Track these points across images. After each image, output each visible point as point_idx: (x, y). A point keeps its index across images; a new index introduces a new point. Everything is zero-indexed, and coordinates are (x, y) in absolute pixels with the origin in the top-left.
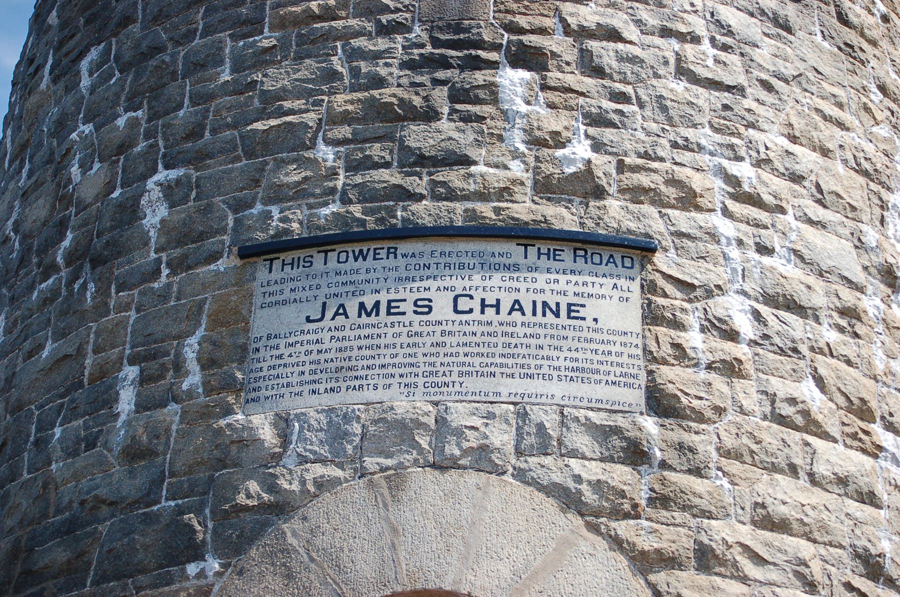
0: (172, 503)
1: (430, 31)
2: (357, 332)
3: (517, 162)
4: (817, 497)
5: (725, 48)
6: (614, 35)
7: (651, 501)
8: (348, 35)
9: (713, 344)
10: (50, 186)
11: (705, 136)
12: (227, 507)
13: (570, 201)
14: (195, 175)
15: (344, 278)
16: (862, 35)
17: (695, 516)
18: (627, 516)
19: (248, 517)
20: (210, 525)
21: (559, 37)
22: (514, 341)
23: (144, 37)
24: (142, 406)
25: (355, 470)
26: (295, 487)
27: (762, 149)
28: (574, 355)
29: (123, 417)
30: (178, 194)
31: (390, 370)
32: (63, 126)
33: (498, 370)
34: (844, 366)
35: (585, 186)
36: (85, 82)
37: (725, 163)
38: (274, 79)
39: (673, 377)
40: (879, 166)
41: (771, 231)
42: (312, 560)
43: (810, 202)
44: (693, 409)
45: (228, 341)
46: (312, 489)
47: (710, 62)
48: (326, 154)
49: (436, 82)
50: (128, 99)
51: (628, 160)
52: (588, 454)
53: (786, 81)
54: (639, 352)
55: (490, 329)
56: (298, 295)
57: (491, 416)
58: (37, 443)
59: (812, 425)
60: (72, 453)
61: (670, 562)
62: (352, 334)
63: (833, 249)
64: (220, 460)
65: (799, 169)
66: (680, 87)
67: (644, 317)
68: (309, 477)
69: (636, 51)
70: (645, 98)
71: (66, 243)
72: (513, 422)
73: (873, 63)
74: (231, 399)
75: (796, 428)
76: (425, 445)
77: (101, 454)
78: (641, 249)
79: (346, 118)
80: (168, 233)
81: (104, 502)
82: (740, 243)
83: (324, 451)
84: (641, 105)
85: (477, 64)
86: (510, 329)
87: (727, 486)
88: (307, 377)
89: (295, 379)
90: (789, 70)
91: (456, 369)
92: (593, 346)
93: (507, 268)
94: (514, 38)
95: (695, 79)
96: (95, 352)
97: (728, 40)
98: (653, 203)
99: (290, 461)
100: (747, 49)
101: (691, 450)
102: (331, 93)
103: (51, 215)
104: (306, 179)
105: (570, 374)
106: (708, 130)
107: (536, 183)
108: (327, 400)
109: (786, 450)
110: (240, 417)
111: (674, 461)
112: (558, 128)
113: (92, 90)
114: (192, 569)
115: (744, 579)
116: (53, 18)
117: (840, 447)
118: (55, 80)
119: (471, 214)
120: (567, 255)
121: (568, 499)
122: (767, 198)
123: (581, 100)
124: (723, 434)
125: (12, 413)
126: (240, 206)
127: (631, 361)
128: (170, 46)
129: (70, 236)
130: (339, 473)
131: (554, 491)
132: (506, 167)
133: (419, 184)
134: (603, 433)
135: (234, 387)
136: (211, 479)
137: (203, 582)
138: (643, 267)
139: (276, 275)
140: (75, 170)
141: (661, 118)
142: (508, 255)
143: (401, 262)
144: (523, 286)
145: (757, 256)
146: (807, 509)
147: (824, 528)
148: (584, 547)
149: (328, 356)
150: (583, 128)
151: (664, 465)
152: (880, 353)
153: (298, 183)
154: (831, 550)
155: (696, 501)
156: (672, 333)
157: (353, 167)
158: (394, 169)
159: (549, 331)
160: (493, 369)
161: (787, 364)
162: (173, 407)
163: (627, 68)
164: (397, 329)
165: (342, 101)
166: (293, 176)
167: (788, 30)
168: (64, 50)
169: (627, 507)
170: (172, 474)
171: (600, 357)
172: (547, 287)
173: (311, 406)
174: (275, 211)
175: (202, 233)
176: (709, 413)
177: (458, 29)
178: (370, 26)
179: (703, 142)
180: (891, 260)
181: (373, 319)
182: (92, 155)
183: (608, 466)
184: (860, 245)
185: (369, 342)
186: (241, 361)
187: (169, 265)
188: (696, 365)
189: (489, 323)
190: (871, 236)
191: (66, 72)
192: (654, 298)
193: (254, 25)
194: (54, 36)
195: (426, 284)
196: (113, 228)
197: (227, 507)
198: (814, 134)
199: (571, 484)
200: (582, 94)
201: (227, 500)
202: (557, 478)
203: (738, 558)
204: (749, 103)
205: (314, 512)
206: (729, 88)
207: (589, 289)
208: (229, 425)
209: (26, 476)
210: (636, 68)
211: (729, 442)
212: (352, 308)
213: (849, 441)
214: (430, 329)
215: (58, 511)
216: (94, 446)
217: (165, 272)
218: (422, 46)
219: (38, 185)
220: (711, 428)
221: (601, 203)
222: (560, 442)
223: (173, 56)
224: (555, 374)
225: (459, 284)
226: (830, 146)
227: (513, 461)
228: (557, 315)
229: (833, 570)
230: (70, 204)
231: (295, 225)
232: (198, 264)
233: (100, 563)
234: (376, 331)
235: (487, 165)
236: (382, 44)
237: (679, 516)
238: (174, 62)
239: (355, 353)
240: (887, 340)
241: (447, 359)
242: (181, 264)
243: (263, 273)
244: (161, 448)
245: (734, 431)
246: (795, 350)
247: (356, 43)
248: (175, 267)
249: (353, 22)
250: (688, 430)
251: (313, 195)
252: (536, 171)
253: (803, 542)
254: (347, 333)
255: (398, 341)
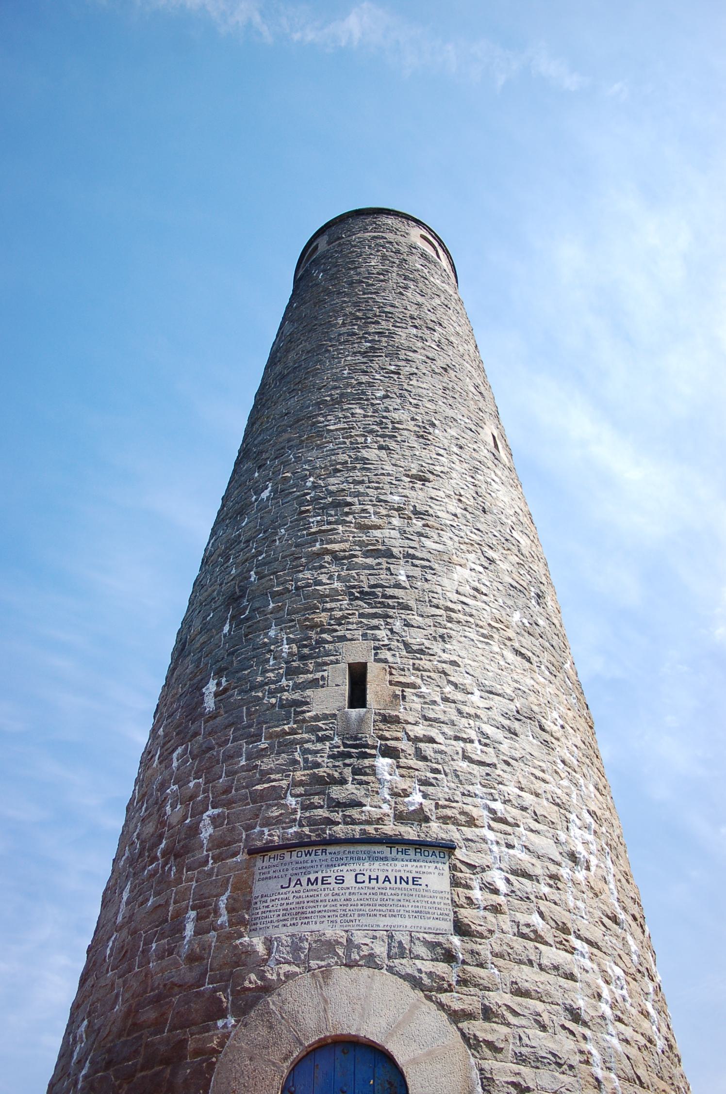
0: (211, 986)
1: (342, 740)
2: (307, 894)
3: (386, 805)
4: (544, 977)
5: (486, 745)
6: (432, 740)
7: (458, 982)
8: (302, 742)
9: (487, 896)
10: (155, 816)
11: (478, 789)
12: (239, 988)
13: (413, 824)
14: (227, 812)
15: (299, 866)
16: (552, 736)
17: (481, 990)
18: (446, 991)
19: (249, 994)
20: (230, 998)
21: (405, 742)
22: (386, 897)
23: (204, 743)
24: (197, 932)
25: (305, 968)
26: (275, 977)
27: (506, 795)
28: (417, 904)
29: (187, 938)
30: (219, 821)
31: (323, 914)
32: (163, 786)
33: (378, 913)
34: (553, 905)
35: (420, 817)
36: (175, 764)
37: (488, 802)
38: (267, 764)
39: (467, 915)
40: (564, 801)
41: (513, 836)
42: (283, 1018)
43: (531, 821)
44: (477, 932)
45: (241, 898)
46: (283, 978)
47: (479, 752)
48: (291, 801)
49: (346, 765)
50: (195, 773)
51: (440, 803)
52: (425, 958)
53: (516, 760)
54: (449, 902)
55: (374, 891)
56: (277, 874)
57: (375, 937)
58: (143, 952)
59: (539, 938)
60: (161, 957)
61: (469, 1016)
62: (304, 895)
63: (544, 844)
64: (236, 962)
65: (525, 804)
66: (465, 765)
67: (451, 883)
68: (282, 972)
69: (443, 748)
70: (447, 771)
71: (162, 846)
72: (386, 941)
73: (558, 749)
74: (242, 929)
75: (531, 940)
76: (341, 954)
77: (175, 959)
78: (448, 848)
79: (301, 783)
80: (213, 842)
81: (176, 985)
82: (498, 843)
83: (289, 957)
84: (446, 775)
85: (365, 756)
86: (384, 891)
87: (497, 972)
88: (281, 918)
89: (275, 919)
90: (517, 755)
91: (356, 913)
92: (426, 899)
93: (382, 859)
94: (383, 742)
95: (472, 761)
96: (174, 903)
97: (487, 741)
98: (453, 824)
99: (272, 963)
100: (497, 745)
101: (477, 953)
102: (294, 771)
103: (155, 831)
104: (281, 814)
105: (415, 914)
106: (479, 786)
107: (395, 815)
108: (291, 930)
109: (526, 952)
110: (247, 939)
111: (469, 961)
112: (405, 787)
113: (178, 768)
114: (220, 1023)
115: (508, 1025)
116: (161, 732)
117: (554, 949)
118: (160, 763)
119: (363, 832)
120: (411, 852)
121: (415, 982)
122: (510, 820)
123: (417, 773)
124: (493, 944)
125: (131, 935)
126: (249, 828)
127: (445, 907)
128: (216, 747)
129: (164, 842)
130: (297, 969)
131: (406, 977)
132: (380, 808)
133: (338, 817)
134: (433, 946)
135: (243, 922)
136: (231, 973)
137: (225, 1030)
138: (450, 857)
139: (266, 864)
140: (168, 808)
141: (456, 780)
142: (382, 852)
143: (329, 857)
144: (390, 868)
145: (506, 850)
146: (539, 984)
147: (548, 994)
148: (424, 1009)
149: (292, 906)
150: (418, 787)
151: (464, 962)
152: (571, 898)
153: (278, 816)
154: (553, 1006)
155: (482, 981)
156: (466, 891)
157: (305, 808)
158: (325, 810)
159: (404, 892)
160: (375, 912)
161: (524, 905)
162: (213, 933)
163: (438, 756)
164: (326, 892)
165: (299, 775)
166: (275, 812)
167: (516, 735)
168: (166, 748)
169: (446, 986)
170: (211, 970)
171: (430, 905)
172: (402, 869)
173: (283, 933)
174: (266, 830)
175: (230, 842)
176: (486, 934)
177: (356, 739)
178: (313, 738)
179: (477, 792)
180: (573, 849)
181: (314, 887)
182: (177, 801)
183: (435, 963)
184: (557, 842)
185: (312, 899)
186: (248, 909)
187: (212, 858)
188: (478, 908)
189: (373, 888)
190: (563, 837)
191: (166, 759)
192: (455, 873)
193: (257, 737)
194: (161, 741)
195: (341, 868)
196: (186, 838)
197: (239, 988)
198: (532, 786)
199: (417, 974)
200: (417, 770)
201: (239, 985)
202: (409, 971)
203: (505, 1013)
204: (499, 772)
205: (285, 991)
206: (489, 765)
207: (423, 869)
208: (241, 943)
209: (137, 970)
210: (443, 756)
211: (497, 949)
212: (304, 881)
213: (558, 946)
214: (344, 891)
215: (152, 990)
216: (172, 954)
217: (211, 862)
218: (339, 747)
219: (150, 815)
220: (487, 941)
221: (428, 825)
222: (410, 952)
223: (218, 752)
224: (407, 914)
225: (358, 868)
226: (539, 792)
227: (387, 962)
228: (407, 883)
229: (554, 1018)
230: (165, 825)
231: (276, 838)
232: (227, 858)
233: (172, 1019)
234: (316, 893)
235: (371, 806)
236: (319, 746)
237: (473, 990)
238: (218, 754)
239: (306, 905)
240: (574, 890)
241: (352, 908)
242: (218, 858)
243: (260, 863)
244: (206, 956)
245: (499, 942)
246: (528, 898)
247: (306, 746)
248: (216, 859)
249: (305, 736)
250: (476, 943)
251: (285, 823)
252: (395, 809)
253: (538, 1003)
254: (301, 894)
255: (327, 898)
